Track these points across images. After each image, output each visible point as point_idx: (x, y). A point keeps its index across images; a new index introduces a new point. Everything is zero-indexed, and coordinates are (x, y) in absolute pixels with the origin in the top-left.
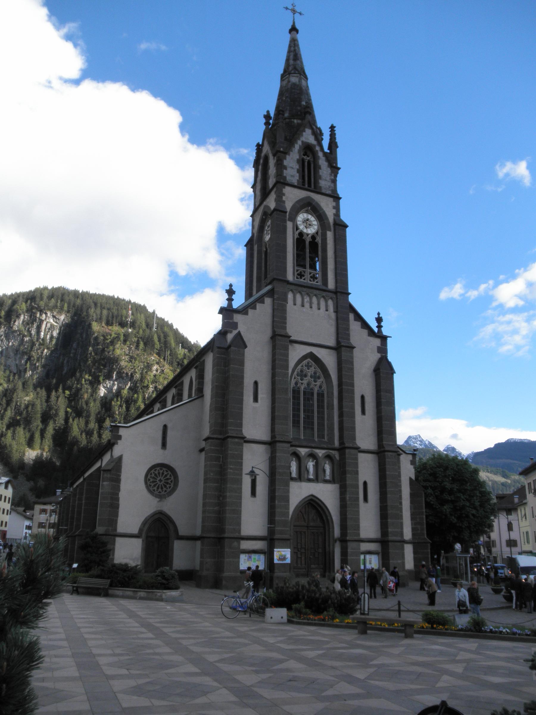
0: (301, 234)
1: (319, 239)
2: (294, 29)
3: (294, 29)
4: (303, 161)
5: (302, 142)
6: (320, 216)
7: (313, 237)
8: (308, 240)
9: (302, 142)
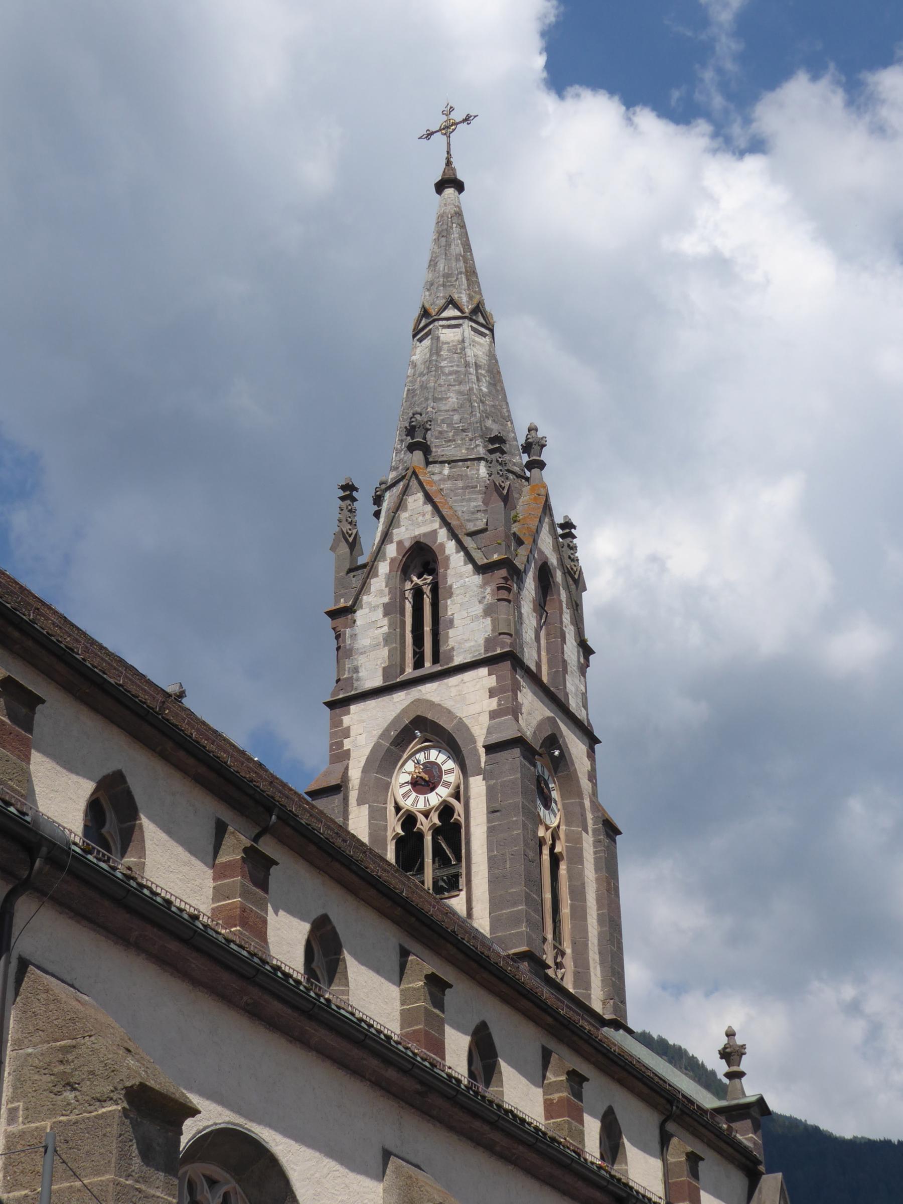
0: (409, 820)
4: (418, 593)
5: (400, 543)
7: (446, 810)
9: (400, 543)
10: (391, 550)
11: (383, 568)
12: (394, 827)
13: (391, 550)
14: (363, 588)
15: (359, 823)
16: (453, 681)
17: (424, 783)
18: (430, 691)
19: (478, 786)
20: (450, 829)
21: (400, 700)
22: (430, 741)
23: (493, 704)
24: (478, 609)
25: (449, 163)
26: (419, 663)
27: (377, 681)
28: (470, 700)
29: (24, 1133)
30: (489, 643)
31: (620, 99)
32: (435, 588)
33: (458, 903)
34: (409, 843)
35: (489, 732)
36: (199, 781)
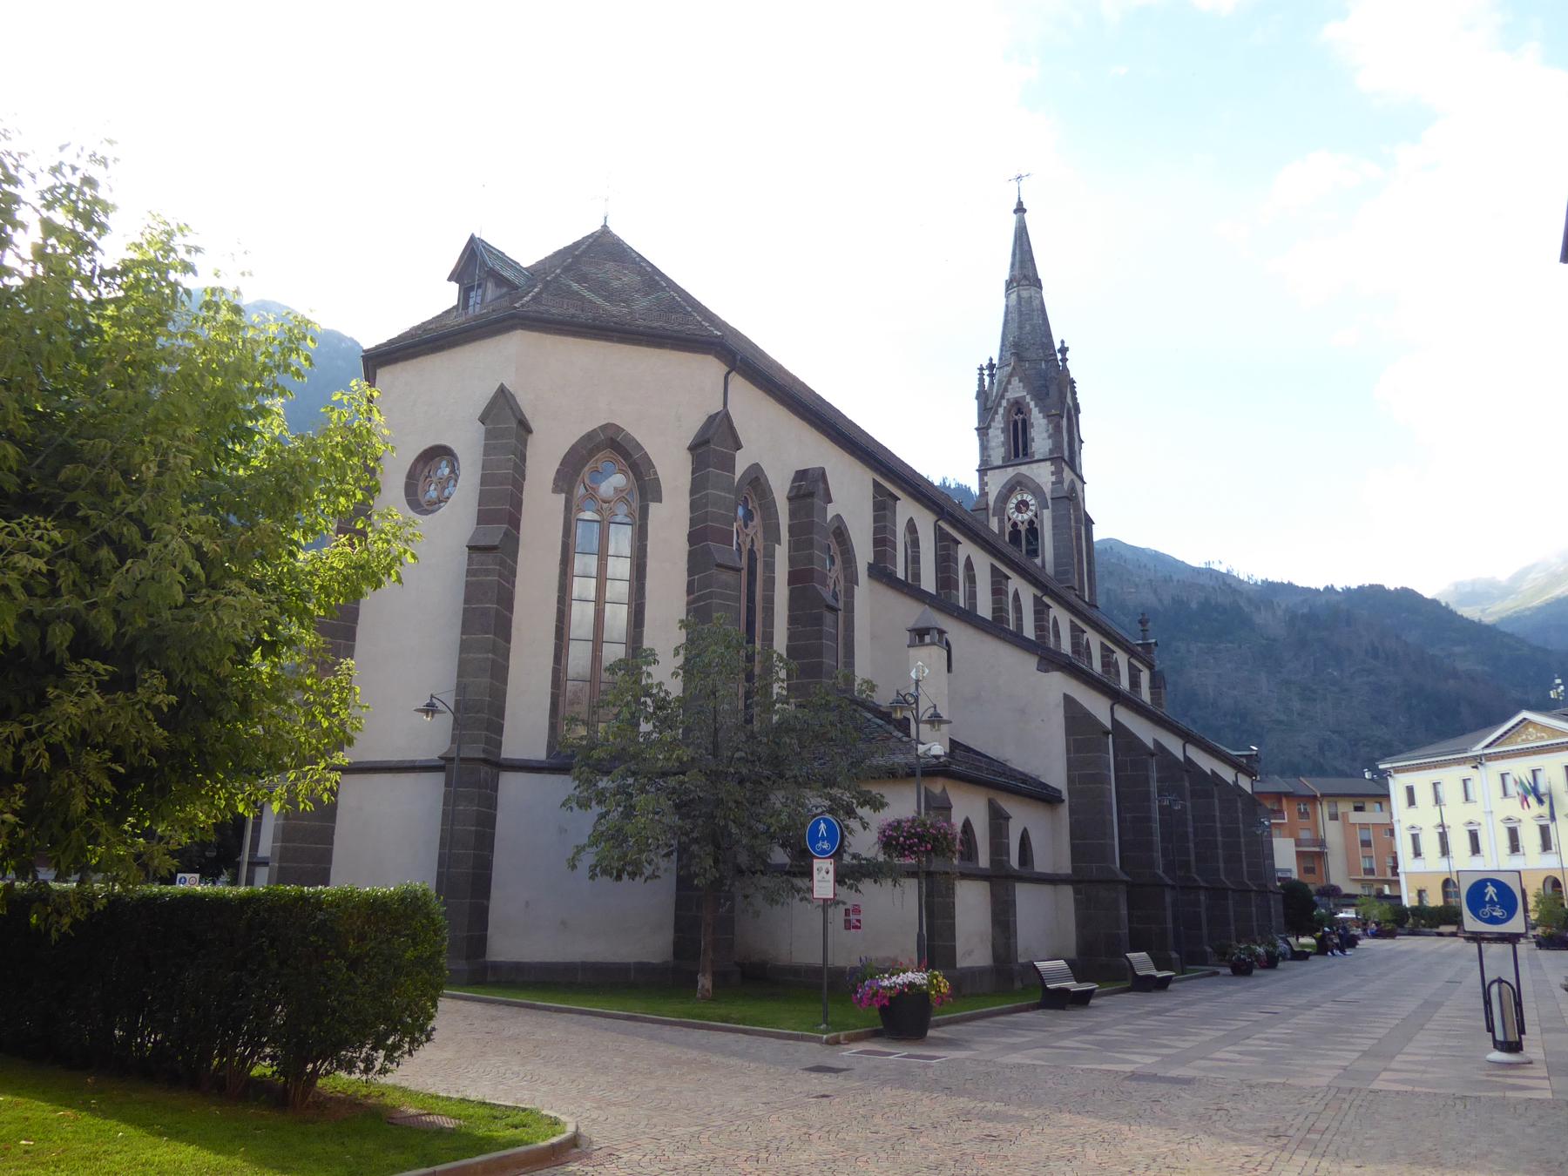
0: (1015, 525)
1: (1037, 525)
2: (1020, 209)
3: (1020, 209)
4: (1016, 423)
6: (1037, 491)
7: (1031, 522)
8: (1023, 528)
10: (1004, 403)
11: (1001, 411)
12: (1008, 528)
13: (1004, 403)
14: (993, 419)
15: (994, 524)
16: (1034, 466)
17: (1022, 506)
18: (1024, 469)
19: (1047, 515)
20: (1033, 531)
21: (1011, 472)
22: (992, 382)
23: (1053, 479)
24: (1045, 435)
25: (1024, 275)
26: (1017, 455)
27: (1000, 463)
28: (1043, 474)
29: (1016, 345)
30: (1051, 451)
31: (931, 484)
32: (1024, 422)
33: (1038, 561)
34: (1015, 535)
35: (1053, 491)
36: (928, 507)
